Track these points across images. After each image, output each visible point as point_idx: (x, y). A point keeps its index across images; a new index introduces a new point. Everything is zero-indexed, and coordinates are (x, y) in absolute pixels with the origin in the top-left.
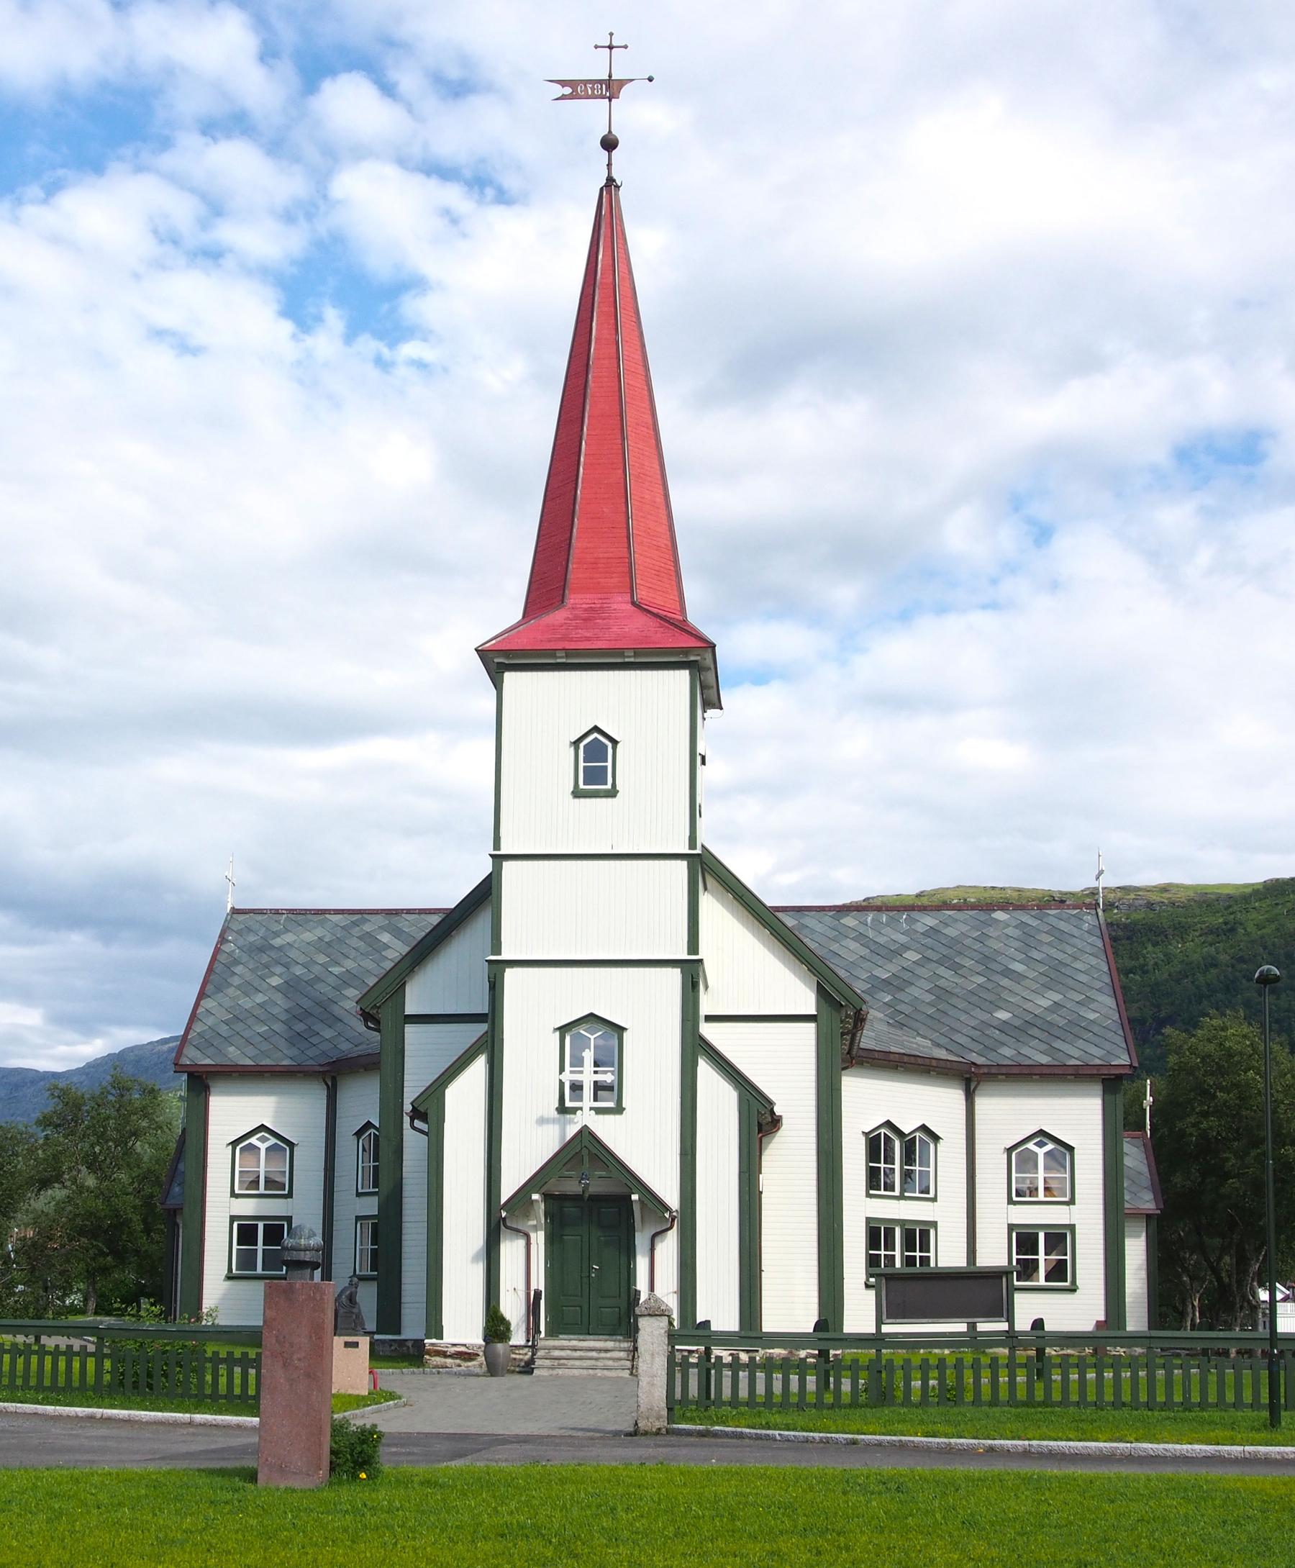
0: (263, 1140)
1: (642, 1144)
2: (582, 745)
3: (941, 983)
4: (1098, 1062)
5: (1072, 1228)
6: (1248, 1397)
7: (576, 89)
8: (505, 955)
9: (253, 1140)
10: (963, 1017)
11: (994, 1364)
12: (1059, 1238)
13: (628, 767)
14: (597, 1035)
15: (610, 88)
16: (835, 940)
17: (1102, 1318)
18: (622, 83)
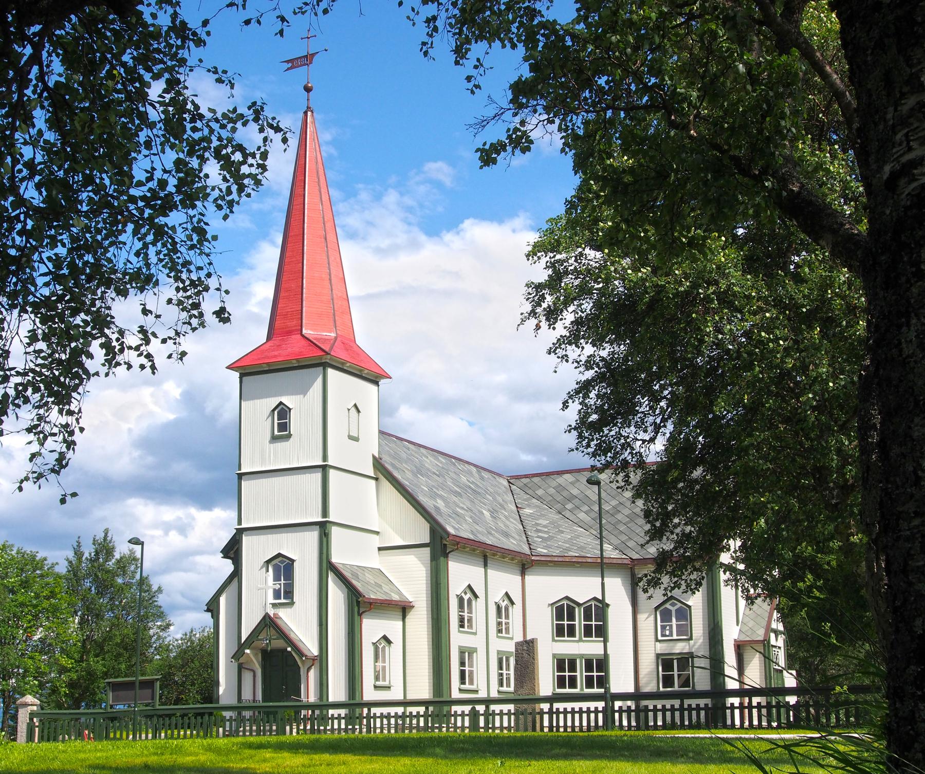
0: (673, 605)
1: (300, 624)
2: (276, 412)
7: (294, 63)
9: (668, 606)
14: (283, 567)
15: (308, 59)
16: (859, 764)
18: (313, 55)
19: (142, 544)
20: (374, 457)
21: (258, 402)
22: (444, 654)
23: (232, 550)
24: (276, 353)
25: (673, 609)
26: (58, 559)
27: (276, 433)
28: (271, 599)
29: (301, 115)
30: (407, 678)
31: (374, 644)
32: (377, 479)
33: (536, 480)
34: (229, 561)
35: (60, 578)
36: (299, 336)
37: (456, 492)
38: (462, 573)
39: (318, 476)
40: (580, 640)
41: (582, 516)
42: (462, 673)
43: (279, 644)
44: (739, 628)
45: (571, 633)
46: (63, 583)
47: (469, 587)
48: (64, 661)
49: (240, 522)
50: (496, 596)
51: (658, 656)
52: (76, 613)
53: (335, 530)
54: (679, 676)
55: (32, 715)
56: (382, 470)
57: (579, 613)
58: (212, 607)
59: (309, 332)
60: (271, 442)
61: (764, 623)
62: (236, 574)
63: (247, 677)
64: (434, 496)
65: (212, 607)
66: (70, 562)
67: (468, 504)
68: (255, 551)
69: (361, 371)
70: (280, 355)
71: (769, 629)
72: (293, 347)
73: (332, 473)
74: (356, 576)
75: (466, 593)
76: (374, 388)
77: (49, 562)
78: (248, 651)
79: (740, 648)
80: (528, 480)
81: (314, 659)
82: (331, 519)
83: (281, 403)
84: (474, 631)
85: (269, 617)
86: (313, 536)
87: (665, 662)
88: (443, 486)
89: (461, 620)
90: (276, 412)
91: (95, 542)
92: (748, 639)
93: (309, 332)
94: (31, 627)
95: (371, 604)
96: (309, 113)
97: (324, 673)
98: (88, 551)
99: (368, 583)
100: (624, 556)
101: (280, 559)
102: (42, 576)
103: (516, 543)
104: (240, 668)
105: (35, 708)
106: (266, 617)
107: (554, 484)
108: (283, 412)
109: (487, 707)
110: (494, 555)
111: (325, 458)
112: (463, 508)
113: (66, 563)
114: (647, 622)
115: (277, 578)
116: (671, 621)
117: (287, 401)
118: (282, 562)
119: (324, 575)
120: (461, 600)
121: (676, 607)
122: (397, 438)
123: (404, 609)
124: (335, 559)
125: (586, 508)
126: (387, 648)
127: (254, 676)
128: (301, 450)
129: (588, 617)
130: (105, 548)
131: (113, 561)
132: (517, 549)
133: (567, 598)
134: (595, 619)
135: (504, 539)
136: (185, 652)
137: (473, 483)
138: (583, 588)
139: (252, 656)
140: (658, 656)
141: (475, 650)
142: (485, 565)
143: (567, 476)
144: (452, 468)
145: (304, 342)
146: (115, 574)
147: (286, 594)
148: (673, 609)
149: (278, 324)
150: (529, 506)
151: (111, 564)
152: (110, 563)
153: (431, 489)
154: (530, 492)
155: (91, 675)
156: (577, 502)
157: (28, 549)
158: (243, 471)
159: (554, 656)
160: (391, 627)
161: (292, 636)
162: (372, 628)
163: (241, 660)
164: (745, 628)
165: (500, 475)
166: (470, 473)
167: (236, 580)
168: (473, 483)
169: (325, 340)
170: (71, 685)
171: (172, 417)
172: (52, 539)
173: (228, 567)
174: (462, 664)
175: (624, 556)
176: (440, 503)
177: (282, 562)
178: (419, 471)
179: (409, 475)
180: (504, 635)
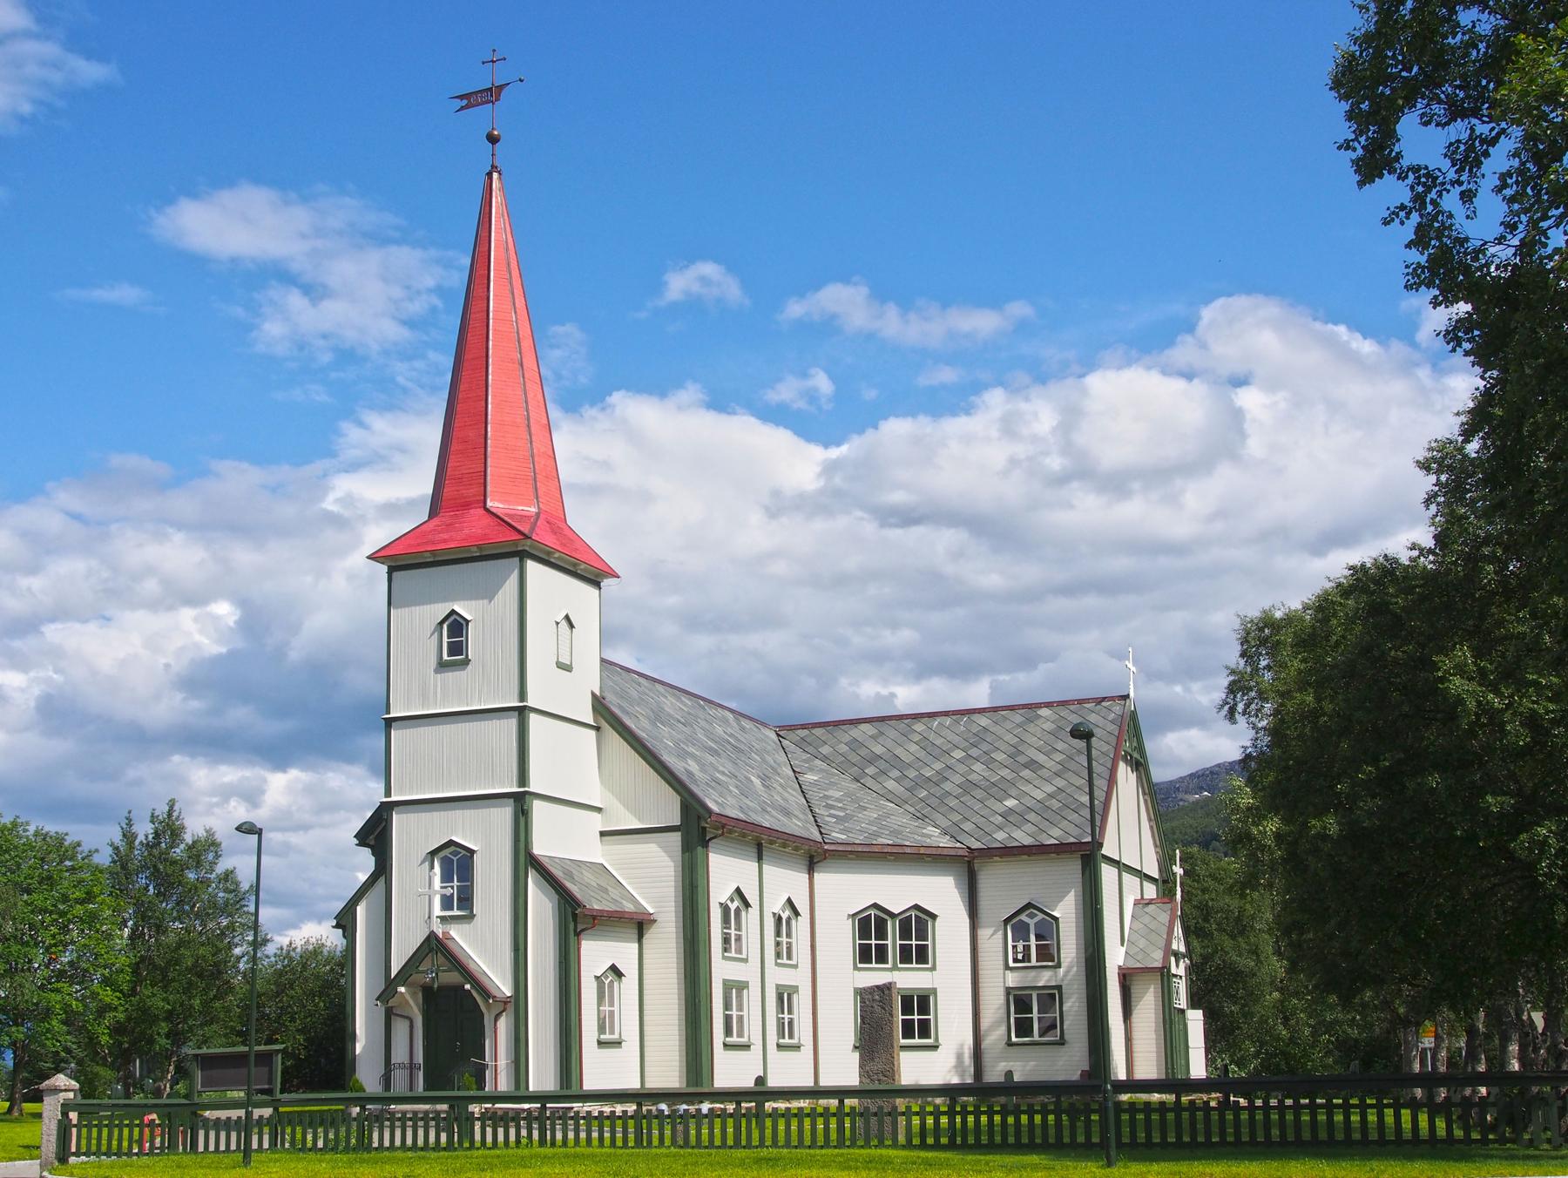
0: (1032, 916)
1: (483, 949)
3: (973, 777)
4: (1072, 840)
5: (934, 991)
6: (233, 1147)
7: (471, 100)
9: (1023, 917)
10: (977, 807)
14: (457, 863)
15: (491, 94)
17: (1087, 1068)
18: (501, 88)
19: (259, 832)
20: (593, 694)
21: (417, 610)
22: (703, 1021)
23: (375, 835)
24: (445, 536)
26: (98, 841)
27: (445, 657)
28: (437, 910)
29: (483, 177)
31: (597, 978)
32: (597, 729)
33: (818, 732)
34: (367, 852)
35: (101, 872)
36: (481, 511)
37: (711, 749)
38: (727, 872)
39: (512, 723)
40: (895, 968)
41: (891, 784)
42: (728, 1020)
43: (453, 978)
44: (1123, 950)
45: (882, 958)
46: (105, 879)
47: (738, 891)
48: (108, 996)
49: (388, 793)
50: (775, 905)
51: (1008, 991)
52: (124, 923)
54: (1040, 1019)
55: (66, 1108)
57: (892, 928)
58: (345, 922)
59: (497, 504)
60: (436, 671)
61: (1162, 943)
62: (383, 868)
63: (400, 1030)
64: (683, 755)
65: (345, 922)
66: (117, 848)
67: (730, 766)
68: (412, 838)
69: (575, 565)
70: (452, 540)
71: (1169, 952)
72: (473, 527)
73: (533, 719)
74: (570, 875)
75: (732, 900)
76: (594, 592)
77: (85, 848)
78: (402, 989)
79: (1126, 977)
81: (506, 1001)
82: (531, 789)
83: (453, 612)
87: (1019, 1001)
88: (692, 740)
89: (726, 940)
91: (153, 818)
92: (1138, 965)
93: (497, 504)
94: (55, 945)
95: (594, 918)
96: (495, 175)
98: (144, 830)
101: (452, 848)
102: (72, 869)
103: (799, 825)
104: (389, 1015)
105: (71, 1095)
107: (847, 738)
108: (457, 626)
109: (841, 1102)
110: (772, 842)
111: (522, 695)
113: (110, 850)
114: (993, 941)
115: (446, 877)
118: (455, 854)
119: (522, 873)
120: (725, 909)
121: (1036, 920)
123: (640, 925)
124: (537, 850)
125: (895, 773)
128: (482, 685)
129: (905, 933)
130: (169, 828)
131: (182, 846)
133: (875, 906)
134: (911, 935)
135: (784, 819)
136: (280, 973)
137: (731, 735)
138: (898, 891)
139: (408, 997)
140: (1008, 991)
141: (795, 989)
142: (760, 859)
143: (863, 727)
144: (701, 714)
145: (488, 520)
146: (184, 867)
147: (464, 900)
148: (1032, 922)
149: (447, 491)
150: (811, 769)
151: (179, 852)
153: (677, 744)
155: (145, 1016)
157: (51, 828)
158: (392, 715)
160: (623, 952)
161: (472, 967)
162: (596, 954)
165: (764, 725)
166: (725, 721)
167: (382, 881)
168: (731, 735)
169: (524, 518)
170: (117, 1030)
171: (224, 650)
172: (91, 811)
173: (365, 861)
174: (727, 1006)
176: (693, 767)
177: (455, 854)
178: (658, 717)
179: (645, 723)
180: (785, 961)
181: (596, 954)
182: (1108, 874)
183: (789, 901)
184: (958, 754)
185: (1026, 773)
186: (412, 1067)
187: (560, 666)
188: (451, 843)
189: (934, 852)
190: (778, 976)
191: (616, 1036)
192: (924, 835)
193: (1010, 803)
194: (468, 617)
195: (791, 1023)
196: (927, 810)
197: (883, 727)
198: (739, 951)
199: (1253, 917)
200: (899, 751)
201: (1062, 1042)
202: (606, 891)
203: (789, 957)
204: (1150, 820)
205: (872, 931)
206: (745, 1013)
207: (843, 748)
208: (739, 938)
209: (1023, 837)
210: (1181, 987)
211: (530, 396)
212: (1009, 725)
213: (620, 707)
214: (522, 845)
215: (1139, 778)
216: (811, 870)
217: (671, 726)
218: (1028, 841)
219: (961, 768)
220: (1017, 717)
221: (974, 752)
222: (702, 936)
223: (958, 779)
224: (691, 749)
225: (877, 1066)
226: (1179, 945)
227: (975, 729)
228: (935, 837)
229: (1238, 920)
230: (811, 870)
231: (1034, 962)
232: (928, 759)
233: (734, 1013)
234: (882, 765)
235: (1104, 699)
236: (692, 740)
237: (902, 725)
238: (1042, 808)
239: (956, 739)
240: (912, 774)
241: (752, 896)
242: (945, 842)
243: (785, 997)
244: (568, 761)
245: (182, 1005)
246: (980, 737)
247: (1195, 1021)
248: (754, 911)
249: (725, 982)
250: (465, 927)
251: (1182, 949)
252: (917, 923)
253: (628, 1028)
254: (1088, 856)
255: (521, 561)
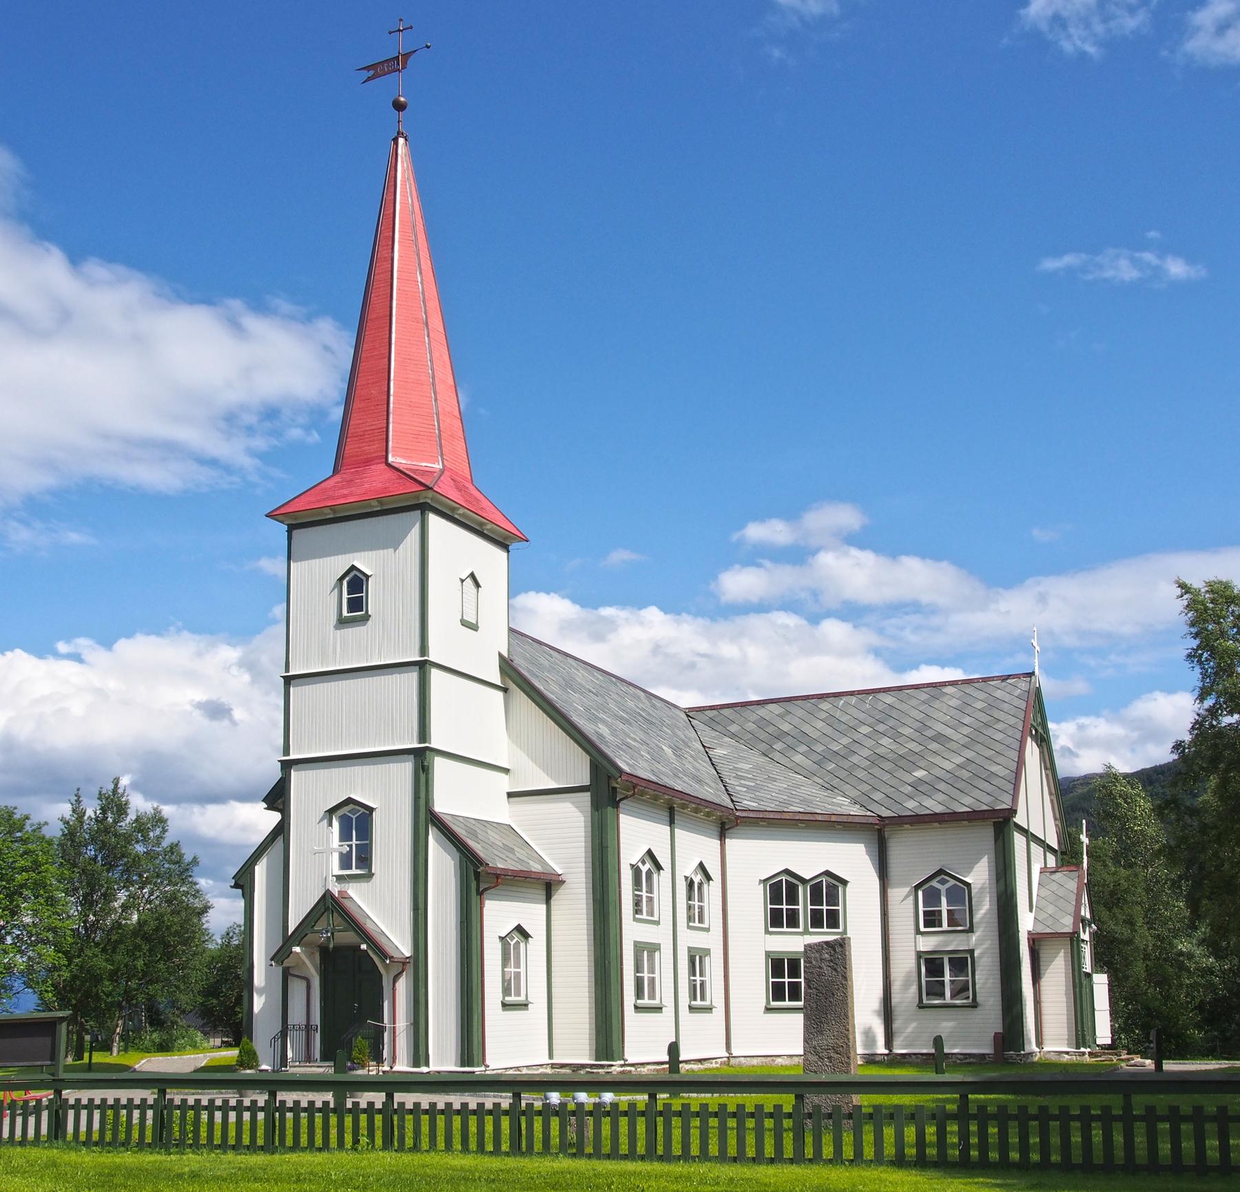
0: (943, 882)
1: (382, 909)
2: (345, 583)
3: (880, 750)
4: (985, 808)
7: (377, 70)
8: (293, 756)
9: (934, 883)
10: (886, 777)
11: (253, 1108)
12: (961, 963)
13: (374, 596)
14: (355, 821)
15: (396, 64)
17: (1001, 1030)
18: (407, 56)
20: (500, 655)
21: (316, 563)
22: (613, 954)
24: (345, 492)
25: (943, 888)
27: (345, 613)
30: (553, 990)
31: (502, 939)
32: (505, 690)
33: (726, 712)
36: (383, 466)
38: (638, 834)
39: (413, 677)
40: (806, 932)
41: (798, 758)
42: (639, 983)
43: (348, 937)
44: (1032, 915)
47: (650, 853)
49: (286, 751)
50: (687, 868)
51: (919, 955)
53: (439, 764)
56: (513, 677)
57: (803, 893)
60: (336, 627)
62: (281, 830)
64: (594, 719)
68: (312, 794)
69: (481, 524)
70: (351, 494)
72: (375, 482)
73: (435, 674)
74: (474, 835)
75: (644, 863)
76: (503, 555)
78: (297, 949)
80: (715, 712)
81: (404, 962)
83: (353, 568)
84: (656, 918)
85: (332, 896)
86: (405, 769)
87: (932, 964)
88: (604, 708)
90: (345, 583)
92: (1048, 931)
95: (498, 876)
96: (401, 141)
97: (421, 984)
98: (91, 810)
99: (492, 845)
100: (869, 813)
101: (351, 806)
103: (710, 792)
104: (286, 975)
106: (327, 897)
107: (754, 717)
108: (356, 582)
110: (684, 807)
111: (424, 649)
112: (635, 740)
115: (345, 836)
116: (939, 903)
117: (364, 562)
119: (422, 831)
120: (637, 872)
121: (948, 885)
122: (533, 639)
123: (548, 886)
124: (440, 807)
125: (803, 748)
126: (522, 945)
127: (309, 988)
128: (383, 638)
129: (816, 897)
132: (717, 801)
133: (787, 872)
138: (809, 857)
139: (304, 957)
140: (919, 955)
141: (707, 952)
142: (672, 823)
143: (771, 707)
144: (613, 688)
145: (390, 474)
147: (360, 859)
148: (943, 888)
149: (349, 449)
150: (721, 746)
152: (123, 824)
153: (587, 709)
154: (719, 728)
156: (789, 740)
159: (768, 954)
160: (531, 913)
161: (369, 926)
162: (499, 916)
163: (287, 963)
164: (1042, 916)
166: (635, 697)
174: (638, 968)
175: (869, 813)
176: (604, 730)
178: (569, 684)
179: (556, 689)
180: (697, 924)
181: (499, 916)
182: (1019, 841)
183: (701, 865)
184: (865, 730)
185: (934, 746)
186: (308, 1028)
187: (465, 623)
188: (349, 801)
189: (845, 819)
190: (690, 939)
191: (522, 998)
192: (833, 804)
193: (920, 774)
194: (369, 573)
195: (702, 984)
196: (836, 782)
197: (788, 705)
198: (651, 913)
199: (1126, 891)
200: (807, 729)
201: (974, 1005)
202: (512, 851)
203: (701, 920)
204: (1050, 794)
205: (783, 896)
206: (657, 975)
207: (750, 726)
208: (650, 900)
209: (933, 805)
210: (1087, 951)
211: (436, 355)
212: (914, 702)
213: (529, 671)
214: (422, 802)
215: (1042, 753)
216: (722, 837)
217: (581, 693)
218: (939, 809)
219: (869, 743)
220: (922, 695)
221: (881, 728)
222: (612, 897)
223: (866, 753)
224: (601, 716)
225: (827, 1040)
226: (1086, 913)
227: (880, 706)
228: (844, 806)
229: (1112, 893)
230: (722, 837)
231: (945, 926)
232: (836, 735)
233: (646, 975)
234: (789, 740)
235: (1009, 677)
236: (604, 708)
237: (808, 705)
238: (952, 779)
239: (862, 716)
240: (819, 748)
241: (663, 858)
242: (855, 810)
243: (696, 959)
244: (471, 719)
245: (126, 966)
246: (886, 715)
247: (1101, 982)
248: (666, 874)
249: (636, 944)
250: (363, 886)
251: (1088, 916)
252: (828, 889)
253: (535, 989)
254: (1001, 824)
255: (423, 514)
